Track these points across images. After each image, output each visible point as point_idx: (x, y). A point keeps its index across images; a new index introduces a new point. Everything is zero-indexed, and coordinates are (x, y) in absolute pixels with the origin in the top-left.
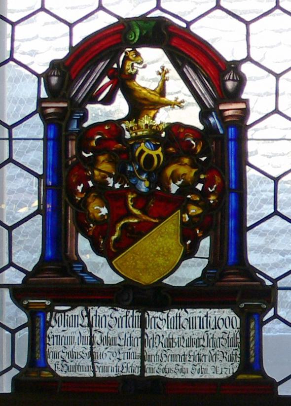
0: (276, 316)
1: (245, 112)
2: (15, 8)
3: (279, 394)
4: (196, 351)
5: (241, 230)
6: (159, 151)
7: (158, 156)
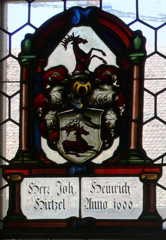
5: (140, 123)
6: (88, 84)
7: (88, 86)
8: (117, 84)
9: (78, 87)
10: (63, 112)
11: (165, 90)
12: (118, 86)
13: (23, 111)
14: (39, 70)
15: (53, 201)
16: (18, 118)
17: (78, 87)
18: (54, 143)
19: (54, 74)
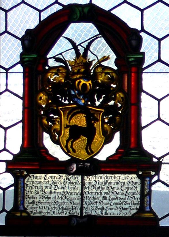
0: (159, 180)
1: (142, 60)
2: (0, 180)
3: (160, 226)
4: (32, 179)
5: (139, 128)
6: (90, 82)
7: (90, 84)
9: (81, 84)
10: (71, 106)
11: (163, 1)
13: (26, 110)
17: (81, 84)
19: (52, 132)
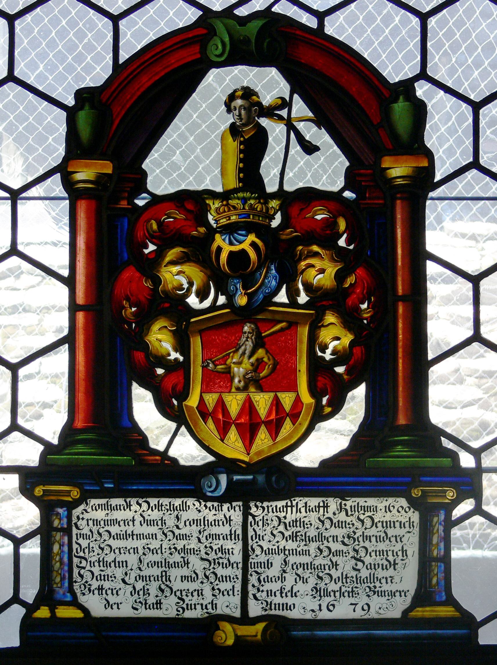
1: (431, 169)
7: (253, 245)
8: (348, 242)
9: (224, 256)
12: (351, 247)
13: (80, 316)
14: (124, 204)
15: (133, 517)
16: (66, 261)
17: (224, 256)
18: (175, 402)
